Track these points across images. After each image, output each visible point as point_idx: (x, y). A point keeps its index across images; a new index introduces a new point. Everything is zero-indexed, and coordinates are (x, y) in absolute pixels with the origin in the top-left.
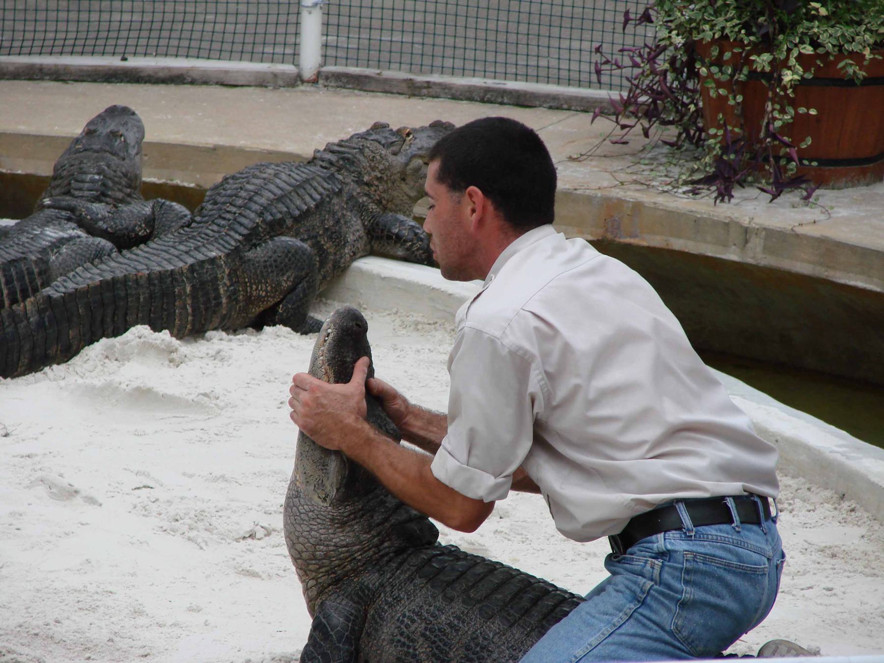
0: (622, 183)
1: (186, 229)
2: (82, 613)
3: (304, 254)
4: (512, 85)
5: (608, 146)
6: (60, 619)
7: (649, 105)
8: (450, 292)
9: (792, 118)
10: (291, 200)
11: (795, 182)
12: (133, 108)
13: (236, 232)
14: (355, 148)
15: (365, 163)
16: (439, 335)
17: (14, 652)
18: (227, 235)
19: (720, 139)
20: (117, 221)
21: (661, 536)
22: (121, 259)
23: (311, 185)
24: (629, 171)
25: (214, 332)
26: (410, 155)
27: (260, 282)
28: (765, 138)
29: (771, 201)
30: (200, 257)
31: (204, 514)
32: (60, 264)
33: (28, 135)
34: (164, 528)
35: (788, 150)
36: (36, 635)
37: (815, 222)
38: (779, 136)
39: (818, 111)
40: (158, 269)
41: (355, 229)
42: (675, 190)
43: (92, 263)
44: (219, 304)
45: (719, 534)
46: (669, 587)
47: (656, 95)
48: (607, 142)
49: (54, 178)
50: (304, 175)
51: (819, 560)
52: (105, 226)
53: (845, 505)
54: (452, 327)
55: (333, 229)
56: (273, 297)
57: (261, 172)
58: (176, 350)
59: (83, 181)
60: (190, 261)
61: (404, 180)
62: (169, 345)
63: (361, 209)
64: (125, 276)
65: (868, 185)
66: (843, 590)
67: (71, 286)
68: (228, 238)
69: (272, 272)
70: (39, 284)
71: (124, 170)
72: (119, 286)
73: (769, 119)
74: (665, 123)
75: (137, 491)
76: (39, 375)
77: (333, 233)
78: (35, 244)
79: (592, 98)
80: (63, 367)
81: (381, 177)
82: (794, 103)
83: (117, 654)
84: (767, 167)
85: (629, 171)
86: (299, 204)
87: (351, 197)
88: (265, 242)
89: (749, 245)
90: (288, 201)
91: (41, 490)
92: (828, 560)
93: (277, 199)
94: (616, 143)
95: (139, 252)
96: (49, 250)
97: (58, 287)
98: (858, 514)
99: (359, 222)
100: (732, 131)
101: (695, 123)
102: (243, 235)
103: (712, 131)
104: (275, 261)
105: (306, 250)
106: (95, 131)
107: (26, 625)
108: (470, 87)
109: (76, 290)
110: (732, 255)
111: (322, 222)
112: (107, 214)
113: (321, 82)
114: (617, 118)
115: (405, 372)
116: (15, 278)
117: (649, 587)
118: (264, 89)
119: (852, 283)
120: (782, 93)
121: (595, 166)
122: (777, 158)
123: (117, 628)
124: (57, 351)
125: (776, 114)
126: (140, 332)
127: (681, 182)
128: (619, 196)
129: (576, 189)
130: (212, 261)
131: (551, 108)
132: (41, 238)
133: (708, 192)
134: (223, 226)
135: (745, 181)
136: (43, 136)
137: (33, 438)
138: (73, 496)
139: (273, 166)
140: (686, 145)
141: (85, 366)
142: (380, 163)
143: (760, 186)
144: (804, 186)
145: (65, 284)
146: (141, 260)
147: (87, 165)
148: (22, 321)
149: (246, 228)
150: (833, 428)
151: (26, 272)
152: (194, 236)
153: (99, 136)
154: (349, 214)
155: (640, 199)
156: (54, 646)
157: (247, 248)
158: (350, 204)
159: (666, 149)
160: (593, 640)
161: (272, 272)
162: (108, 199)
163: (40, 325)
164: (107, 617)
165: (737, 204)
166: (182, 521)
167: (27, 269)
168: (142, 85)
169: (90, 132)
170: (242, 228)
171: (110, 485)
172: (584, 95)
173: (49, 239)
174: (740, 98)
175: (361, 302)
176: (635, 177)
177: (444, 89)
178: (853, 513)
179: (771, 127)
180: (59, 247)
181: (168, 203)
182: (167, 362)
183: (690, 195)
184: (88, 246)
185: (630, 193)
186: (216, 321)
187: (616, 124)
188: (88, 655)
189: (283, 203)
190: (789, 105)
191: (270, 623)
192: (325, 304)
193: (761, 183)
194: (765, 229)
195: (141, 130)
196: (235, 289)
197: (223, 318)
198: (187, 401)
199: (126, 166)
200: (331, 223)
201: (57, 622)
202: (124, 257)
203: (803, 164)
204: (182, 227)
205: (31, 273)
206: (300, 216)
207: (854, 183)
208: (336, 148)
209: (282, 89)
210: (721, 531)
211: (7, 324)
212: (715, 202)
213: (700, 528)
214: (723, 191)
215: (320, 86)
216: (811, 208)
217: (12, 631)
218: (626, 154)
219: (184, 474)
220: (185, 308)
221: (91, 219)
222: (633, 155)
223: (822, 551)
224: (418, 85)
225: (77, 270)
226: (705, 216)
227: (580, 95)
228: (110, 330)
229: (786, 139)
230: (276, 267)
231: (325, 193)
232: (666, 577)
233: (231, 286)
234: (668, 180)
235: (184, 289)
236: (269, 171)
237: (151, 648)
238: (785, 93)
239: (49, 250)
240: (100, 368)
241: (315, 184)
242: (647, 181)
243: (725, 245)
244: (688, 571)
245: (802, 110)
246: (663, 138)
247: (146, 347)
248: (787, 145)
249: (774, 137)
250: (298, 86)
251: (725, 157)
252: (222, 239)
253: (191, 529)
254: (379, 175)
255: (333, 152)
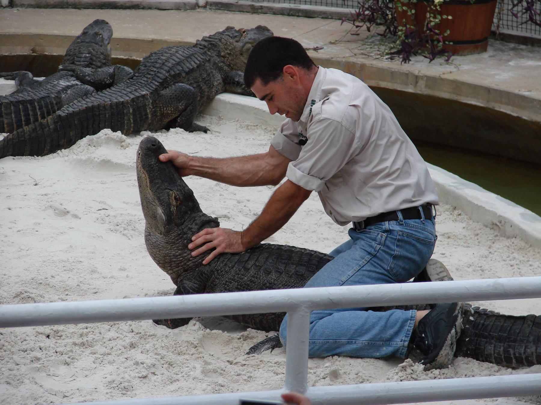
0: (355, 55)
1: (131, 80)
2: (65, 272)
3: (190, 92)
4: (303, 7)
5: (349, 37)
6: (54, 275)
7: (370, 16)
8: (264, 110)
9: (440, 21)
10: (184, 64)
11: (441, 53)
12: (107, 20)
13: (156, 81)
14: (217, 39)
15: (222, 46)
16: (259, 131)
17: (29, 292)
18: (151, 82)
19: (404, 32)
20: (96, 76)
21: (387, 223)
22: (97, 96)
23: (194, 57)
24: (360, 48)
25: (145, 132)
26: (245, 42)
27: (168, 106)
28: (426, 31)
29: (430, 62)
30: (137, 94)
31: (132, 222)
32: (67, 99)
33: (59, 36)
34: (112, 229)
35: (438, 37)
36: (41, 283)
37: (451, 72)
38: (433, 30)
39: (452, 17)
40: (116, 101)
41: (218, 78)
42: (382, 58)
43: (82, 99)
44: (147, 118)
45: (415, 224)
46: (388, 247)
47: (373, 10)
48: (349, 34)
49: (66, 55)
50: (191, 52)
51: (441, 240)
52: (89, 79)
53: (456, 212)
54: (265, 128)
55: (207, 79)
56: (175, 114)
57: (169, 50)
58: (124, 141)
59: (81, 58)
60: (132, 96)
61: (241, 54)
62: (121, 139)
63: (220, 69)
64: (98, 104)
65: (479, 53)
66: (450, 254)
67: (71, 110)
68: (151, 84)
69: (174, 101)
70: (56, 109)
71: (101, 51)
72: (95, 109)
73: (428, 21)
74: (378, 24)
75: (99, 211)
76: (55, 154)
77: (206, 81)
78: (54, 89)
79: (343, 13)
80: (67, 150)
81: (230, 53)
82: (441, 14)
83: (81, 292)
84: (427, 45)
85: (360, 48)
86: (188, 66)
87: (215, 63)
88: (171, 86)
89: (418, 84)
90: (183, 64)
91: (50, 211)
92: (446, 240)
93: (177, 64)
94: (353, 34)
95: (106, 92)
96: (61, 92)
97: (64, 110)
98: (462, 217)
99: (219, 75)
100: (410, 28)
101: (393, 24)
102: (159, 83)
103: (400, 28)
104: (176, 95)
105: (192, 90)
106: (87, 32)
107: (36, 279)
108: (282, 8)
109: (73, 111)
110: (410, 89)
111: (201, 75)
112: (90, 73)
113: (208, 7)
114: (354, 23)
115: (240, 150)
116: (44, 106)
117: (378, 248)
118: (179, 11)
119: (469, 102)
120: (434, 8)
121: (344, 47)
122: (433, 41)
123: (81, 280)
124: (64, 142)
125: (432, 19)
126: (106, 132)
127: (385, 53)
128: (354, 61)
129: (332, 58)
130: (143, 96)
131: (322, 18)
132: (57, 86)
133: (398, 58)
134: (149, 78)
135: (417, 53)
136: (66, 36)
137: (49, 186)
138: (66, 214)
139: (175, 48)
140: (389, 35)
141: (79, 150)
142: (229, 46)
143: (424, 55)
144: (446, 54)
145: (68, 109)
146: (107, 96)
147: (82, 49)
148: (46, 128)
149: (161, 79)
150: (451, 174)
151: (49, 103)
152: (135, 84)
153: (89, 35)
154: (214, 71)
155: (364, 63)
156: (50, 289)
157: (162, 89)
158: (215, 66)
159: (379, 37)
160: (350, 273)
161: (174, 101)
162: (93, 66)
163: (56, 129)
164: (78, 274)
165: (413, 64)
166: (120, 226)
167: (50, 101)
168: (118, 10)
169: (84, 33)
170: (159, 79)
171: (85, 208)
172: (339, 11)
173: (61, 86)
174: (413, 11)
175: (221, 116)
176: (362, 51)
177: (269, 9)
178: (459, 216)
179: (429, 25)
180: (67, 90)
181: (122, 67)
182: (120, 147)
183: (389, 60)
184: (81, 89)
185: (359, 59)
186: (146, 126)
187: (353, 25)
188: (67, 293)
189: (180, 66)
190: (438, 14)
191: (160, 276)
192: (203, 117)
193: (425, 53)
194: (426, 76)
195: (111, 32)
196: (155, 110)
197: (149, 125)
198: (128, 166)
199: (102, 50)
200: (205, 76)
201: (53, 277)
202: (98, 95)
203: (446, 44)
204: (129, 79)
205: (52, 104)
206: (189, 71)
207: (471, 53)
208: (208, 39)
209: (188, 11)
210: (416, 222)
211: (38, 129)
212: (401, 63)
213: (407, 221)
214: (406, 58)
215: (208, 9)
216: (450, 65)
217: (28, 281)
218: (359, 40)
219: (124, 202)
220: (129, 120)
221: (83, 75)
222: (362, 40)
223: (443, 235)
224: (256, 7)
225: (74, 102)
226: (396, 70)
227: (337, 11)
228: (92, 131)
229: (437, 31)
230: (176, 98)
231: (202, 60)
232: (388, 243)
233: (153, 108)
234: (379, 52)
235: (129, 110)
236: (173, 50)
237: (98, 289)
238: (436, 8)
239: (61, 92)
240: (86, 150)
241: (196, 56)
242: (368, 53)
243: (406, 84)
244: (399, 240)
245: (445, 17)
246: (377, 32)
247: (109, 140)
248: (437, 34)
249: (431, 30)
250: (196, 9)
251: (406, 41)
252: (149, 85)
253: (125, 229)
254: (229, 52)
255: (206, 41)
